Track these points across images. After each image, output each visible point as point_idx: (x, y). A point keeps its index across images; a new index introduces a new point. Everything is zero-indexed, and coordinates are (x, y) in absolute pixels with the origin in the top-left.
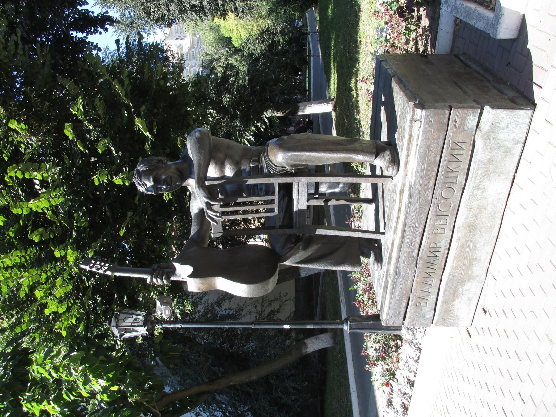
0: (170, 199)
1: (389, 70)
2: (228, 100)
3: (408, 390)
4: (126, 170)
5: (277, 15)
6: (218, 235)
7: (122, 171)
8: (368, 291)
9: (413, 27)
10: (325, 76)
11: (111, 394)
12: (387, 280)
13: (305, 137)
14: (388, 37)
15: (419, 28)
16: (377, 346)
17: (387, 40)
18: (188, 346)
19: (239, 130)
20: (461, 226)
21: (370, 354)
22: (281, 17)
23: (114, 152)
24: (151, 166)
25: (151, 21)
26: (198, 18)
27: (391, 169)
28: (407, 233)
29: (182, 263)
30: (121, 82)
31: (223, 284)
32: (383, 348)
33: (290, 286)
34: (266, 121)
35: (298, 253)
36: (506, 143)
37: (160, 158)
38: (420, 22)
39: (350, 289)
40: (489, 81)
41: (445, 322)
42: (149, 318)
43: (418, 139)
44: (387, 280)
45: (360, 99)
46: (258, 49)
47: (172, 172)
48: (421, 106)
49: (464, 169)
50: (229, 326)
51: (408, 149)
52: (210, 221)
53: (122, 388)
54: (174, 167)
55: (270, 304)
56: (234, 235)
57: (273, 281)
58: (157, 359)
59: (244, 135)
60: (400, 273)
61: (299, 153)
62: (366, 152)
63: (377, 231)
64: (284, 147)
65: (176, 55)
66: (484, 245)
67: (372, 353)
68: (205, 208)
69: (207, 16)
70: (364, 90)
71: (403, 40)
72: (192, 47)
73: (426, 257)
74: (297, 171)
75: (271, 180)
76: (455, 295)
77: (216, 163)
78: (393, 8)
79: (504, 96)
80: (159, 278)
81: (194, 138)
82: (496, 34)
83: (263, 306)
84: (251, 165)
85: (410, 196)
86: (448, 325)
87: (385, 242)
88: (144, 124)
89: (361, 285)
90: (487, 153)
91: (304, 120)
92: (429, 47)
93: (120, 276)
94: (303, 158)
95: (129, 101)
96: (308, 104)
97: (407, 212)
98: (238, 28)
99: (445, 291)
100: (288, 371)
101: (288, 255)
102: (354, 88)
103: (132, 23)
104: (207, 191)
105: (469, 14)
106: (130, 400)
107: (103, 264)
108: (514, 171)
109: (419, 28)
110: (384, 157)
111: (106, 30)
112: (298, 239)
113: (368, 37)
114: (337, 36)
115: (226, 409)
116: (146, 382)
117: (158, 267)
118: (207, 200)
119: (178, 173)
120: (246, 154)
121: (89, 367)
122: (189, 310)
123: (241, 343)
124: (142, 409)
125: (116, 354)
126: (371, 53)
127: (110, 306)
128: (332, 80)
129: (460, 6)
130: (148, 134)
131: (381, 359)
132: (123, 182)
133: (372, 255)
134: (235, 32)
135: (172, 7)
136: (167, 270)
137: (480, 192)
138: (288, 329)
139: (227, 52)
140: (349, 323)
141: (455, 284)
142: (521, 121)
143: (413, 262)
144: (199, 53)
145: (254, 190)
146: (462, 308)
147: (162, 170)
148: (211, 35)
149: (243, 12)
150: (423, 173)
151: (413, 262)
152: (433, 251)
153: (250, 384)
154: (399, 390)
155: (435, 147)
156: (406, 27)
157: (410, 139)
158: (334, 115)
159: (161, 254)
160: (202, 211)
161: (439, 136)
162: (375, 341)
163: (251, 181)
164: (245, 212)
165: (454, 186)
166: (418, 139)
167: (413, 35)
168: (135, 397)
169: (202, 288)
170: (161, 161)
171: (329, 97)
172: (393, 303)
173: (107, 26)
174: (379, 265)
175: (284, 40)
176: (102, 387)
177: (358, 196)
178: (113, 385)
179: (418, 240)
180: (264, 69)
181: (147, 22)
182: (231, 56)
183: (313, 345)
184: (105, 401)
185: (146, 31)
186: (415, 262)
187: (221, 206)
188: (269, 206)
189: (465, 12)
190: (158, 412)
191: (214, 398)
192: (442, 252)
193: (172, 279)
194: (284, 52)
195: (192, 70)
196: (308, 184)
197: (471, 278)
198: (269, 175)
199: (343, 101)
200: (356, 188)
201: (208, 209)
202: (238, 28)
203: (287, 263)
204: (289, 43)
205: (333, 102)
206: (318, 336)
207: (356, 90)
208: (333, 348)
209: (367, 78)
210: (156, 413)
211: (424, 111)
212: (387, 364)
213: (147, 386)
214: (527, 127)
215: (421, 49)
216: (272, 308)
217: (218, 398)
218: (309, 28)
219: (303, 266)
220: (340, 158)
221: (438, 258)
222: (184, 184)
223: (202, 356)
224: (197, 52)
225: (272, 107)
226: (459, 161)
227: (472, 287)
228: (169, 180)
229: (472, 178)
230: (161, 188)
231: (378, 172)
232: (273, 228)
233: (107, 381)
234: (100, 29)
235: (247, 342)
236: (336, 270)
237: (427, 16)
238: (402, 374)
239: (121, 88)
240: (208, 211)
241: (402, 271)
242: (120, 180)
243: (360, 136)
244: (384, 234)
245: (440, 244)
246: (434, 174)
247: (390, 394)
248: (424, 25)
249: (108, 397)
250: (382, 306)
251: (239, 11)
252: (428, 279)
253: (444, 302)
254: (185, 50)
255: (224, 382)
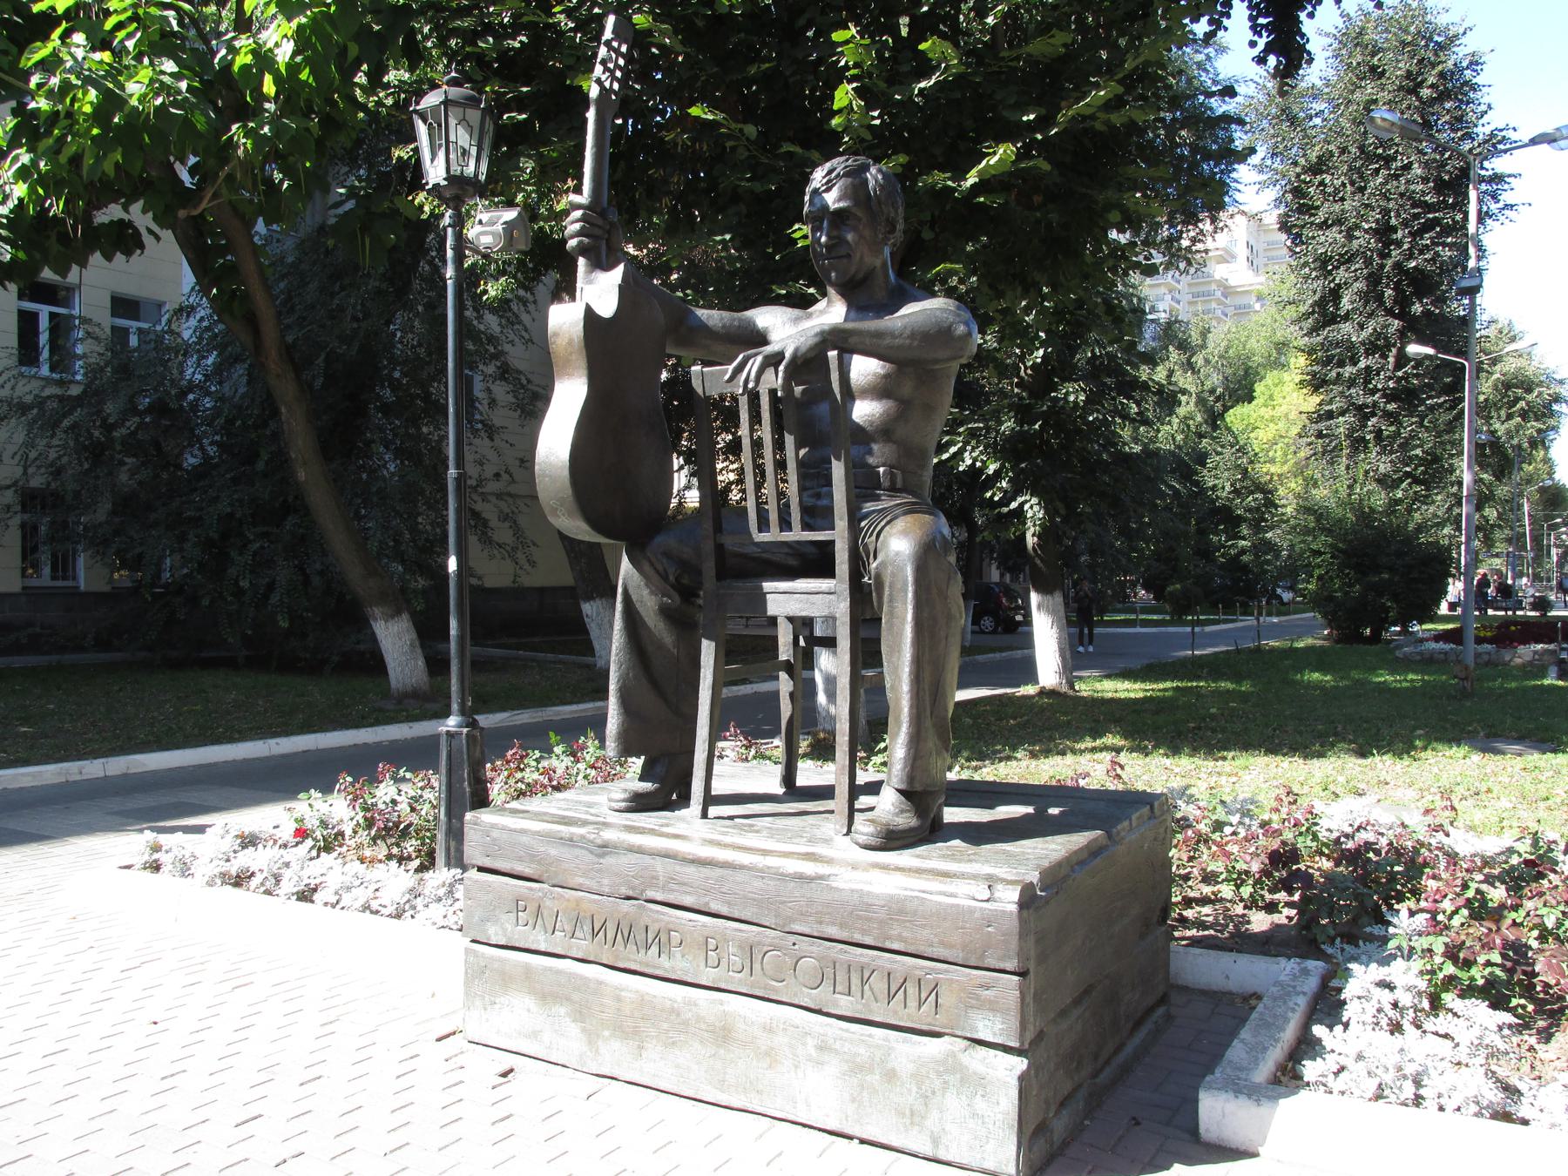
0: (795, 241)
1: (1126, 823)
2: (1072, 398)
3: (288, 886)
4: (874, 118)
5: (1307, 531)
6: (696, 384)
7: (869, 107)
8: (550, 780)
9: (1246, 891)
10: (1136, 664)
11: (252, 76)
12: (585, 823)
13: (954, 610)
14: (1228, 830)
15: (1245, 907)
16: (404, 807)
17: (1218, 826)
18: (384, 286)
19: (988, 429)
20: (726, 1008)
21: (382, 786)
22: (1303, 542)
23: (922, 85)
24: (879, 203)
25: (1298, 176)
26: (1303, 309)
27: (870, 829)
28: (706, 871)
29: (623, 289)
30: (1114, 104)
31: (569, 397)
32: (397, 825)
33: (553, 571)
34: (1014, 505)
35: (652, 593)
36: (934, 1115)
37: (900, 226)
38: (1262, 908)
39: (552, 734)
40: (1095, 1075)
41: (476, 974)
42: (471, 189)
43: (944, 894)
44: (585, 823)
45: (1069, 758)
46: (1219, 480)
47: (862, 258)
48: (1028, 900)
49: (870, 1011)
50: (451, 410)
51: (919, 871)
52: (735, 364)
53: (267, 105)
54: (878, 263)
55: (504, 517)
56: (694, 420)
57: (579, 529)
58: (350, 205)
59: (973, 442)
60: (602, 855)
61: (910, 595)
62: (913, 767)
63: (710, 800)
64: (926, 557)
65: (1199, 246)
66: (677, 1066)
67: (385, 792)
68: (768, 349)
69: (1309, 334)
70: (1090, 767)
71: (1217, 866)
72: (1228, 291)
73: (645, 920)
74: (866, 590)
75: (841, 523)
76: (548, 995)
77: (886, 376)
78: (1300, 839)
79: (1053, 1108)
80: (582, 228)
81: (951, 319)
82: (1210, 1088)
83: (499, 496)
84: (881, 470)
85: (800, 877)
86: (468, 983)
87: (682, 819)
88: (1001, 170)
89: (563, 765)
90: (911, 1067)
91: (1018, 608)
92: (1194, 932)
93: (585, 121)
94: (898, 604)
95: (1063, 127)
96: (1059, 620)
97: (761, 871)
98: (1278, 420)
99: (559, 972)
100: (318, 566)
101: (647, 567)
102: (1098, 742)
103: (1293, 121)
104: (812, 354)
105: (1268, 1026)
106: (234, 127)
107: (618, 74)
108: (864, 1136)
109: (1245, 907)
110: (902, 811)
111: (1261, 60)
112: (688, 593)
113: (1234, 779)
114: (1244, 697)
115: (208, 394)
116: (287, 172)
117: (612, 224)
118: (788, 355)
119: (861, 275)
120: (910, 456)
121: (327, 15)
122: (485, 292)
123: (395, 435)
124: (212, 162)
125: (361, 87)
126: (1188, 787)
127: (496, 72)
128: (1127, 685)
129: (1291, 1004)
130: (972, 179)
131: (369, 815)
132: (840, 111)
133: (648, 786)
134: (1266, 413)
135: (1334, 234)
136: (604, 247)
137: (813, 1052)
138: (446, 567)
139: (1212, 391)
140: (465, 730)
141: (576, 996)
142: (990, 1147)
143: (633, 888)
144: (1209, 312)
145: (815, 477)
146: (514, 1017)
147: (867, 233)
148: (1258, 346)
149: (1320, 435)
150: (860, 909)
151: (633, 888)
152: (661, 940)
153: (281, 461)
154: (287, 865)
155: (922, 939)
156: (1247, 873)
157: (946, 875)
158: (1029, 690)
159: (643, 214)
160: (761, 339)
161: (951, 946)
162: (416, 799)
163: (838, 470)
164: (757, 445)
165: (826, 987)
166: (944, 894)
167: (1227, 891)
168: (244, 144)
169: (559, 341)
170: (893, 230)
171: (1080, 678)
172: (524, 839)
173: (1272, 60)
174: (623, 804)
175: (1243, 551)
176: (270, 50)
177: (805, 756)
178: (278, 80)
179: (688, 901)
180: (1163, 496)
181: (1295, 164)
182: (1201, 401)
183: (394, 638)
184: (233, 61)
185: (1269, 162)
186: (631, 893)
187: (773, 392)
188: (773, 517)
189: (1275, 1016)
190: (204, 205)
191: (237, 359)
192: (657, 961)
193: (581, 261)
194: (1206, 552)
195: (1163, 290)
196: (831, 619)
197: (591, 1037)
198: (854, 518)
199: (1065, 714)
200: (823, 751)
201: (766, 358)
202: (1278, 420)
203: (625, 564)
204: (1234, 563)
205: (1064, 689)
206: (419, 651)
207: (1093, 750)
208: (386, 692)
209: (1118, 776)
210: (201, 199)
211: (1014, 908)
212: (355, 832)
213: (277, 176)
214: (974, 1165)
215: (1189, 913)
216: (494, 522)
217: (240, 370)
218: (1275, 620)
219: (619, 606)
220: (898, 700)
221: (643, 951)
222: (831, 291)
223: (355, 325)
224: (1214, 305)
225: (1052, 520)
226: (890, 997)
227: (567, 1039)
228: (842, 251)
229: (847, 1031)
230: (820, 229)
231: (864, 801)
232: (718, 528)
233: (288, 65)
234: (1262, 43)
235: (399, 453)
236: (607, 699)
237: (1277, 927)
238: (332, 870)
239: (1101, 102)
240: (759, 359)
241: (609, 861)
242: (845, 103)
243: (968, 760)
244: (704, 815)
245: (678, 955)
246: (858, 938)
247: (275, 841)
248: (1252, 919)
249: (245, 68)
250: (515, 812)
251: (1322, 426)
252: (587, 928)
253: (528, 970)
254: (1219, 271)
255: (286, 389)
